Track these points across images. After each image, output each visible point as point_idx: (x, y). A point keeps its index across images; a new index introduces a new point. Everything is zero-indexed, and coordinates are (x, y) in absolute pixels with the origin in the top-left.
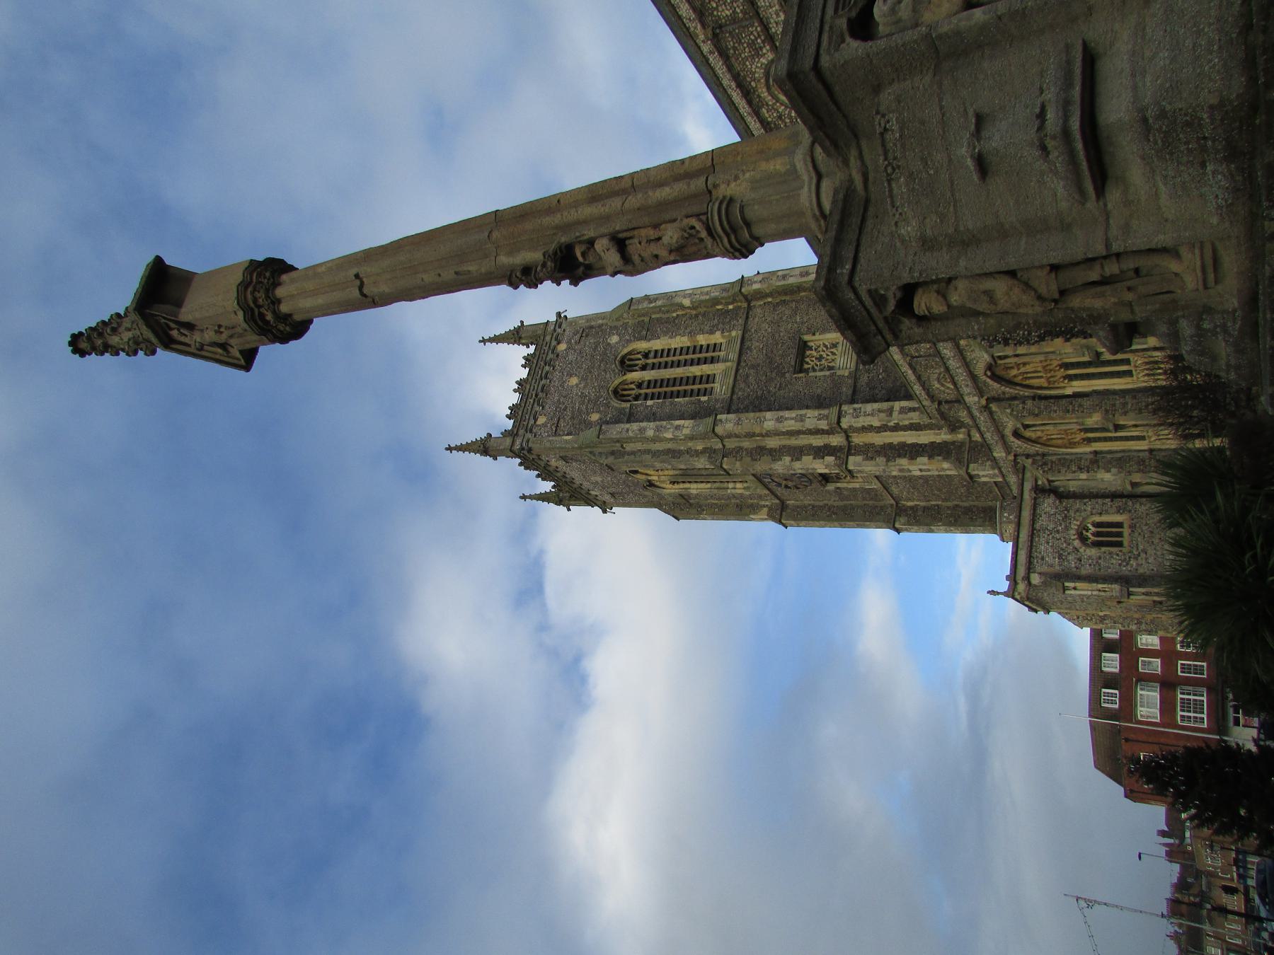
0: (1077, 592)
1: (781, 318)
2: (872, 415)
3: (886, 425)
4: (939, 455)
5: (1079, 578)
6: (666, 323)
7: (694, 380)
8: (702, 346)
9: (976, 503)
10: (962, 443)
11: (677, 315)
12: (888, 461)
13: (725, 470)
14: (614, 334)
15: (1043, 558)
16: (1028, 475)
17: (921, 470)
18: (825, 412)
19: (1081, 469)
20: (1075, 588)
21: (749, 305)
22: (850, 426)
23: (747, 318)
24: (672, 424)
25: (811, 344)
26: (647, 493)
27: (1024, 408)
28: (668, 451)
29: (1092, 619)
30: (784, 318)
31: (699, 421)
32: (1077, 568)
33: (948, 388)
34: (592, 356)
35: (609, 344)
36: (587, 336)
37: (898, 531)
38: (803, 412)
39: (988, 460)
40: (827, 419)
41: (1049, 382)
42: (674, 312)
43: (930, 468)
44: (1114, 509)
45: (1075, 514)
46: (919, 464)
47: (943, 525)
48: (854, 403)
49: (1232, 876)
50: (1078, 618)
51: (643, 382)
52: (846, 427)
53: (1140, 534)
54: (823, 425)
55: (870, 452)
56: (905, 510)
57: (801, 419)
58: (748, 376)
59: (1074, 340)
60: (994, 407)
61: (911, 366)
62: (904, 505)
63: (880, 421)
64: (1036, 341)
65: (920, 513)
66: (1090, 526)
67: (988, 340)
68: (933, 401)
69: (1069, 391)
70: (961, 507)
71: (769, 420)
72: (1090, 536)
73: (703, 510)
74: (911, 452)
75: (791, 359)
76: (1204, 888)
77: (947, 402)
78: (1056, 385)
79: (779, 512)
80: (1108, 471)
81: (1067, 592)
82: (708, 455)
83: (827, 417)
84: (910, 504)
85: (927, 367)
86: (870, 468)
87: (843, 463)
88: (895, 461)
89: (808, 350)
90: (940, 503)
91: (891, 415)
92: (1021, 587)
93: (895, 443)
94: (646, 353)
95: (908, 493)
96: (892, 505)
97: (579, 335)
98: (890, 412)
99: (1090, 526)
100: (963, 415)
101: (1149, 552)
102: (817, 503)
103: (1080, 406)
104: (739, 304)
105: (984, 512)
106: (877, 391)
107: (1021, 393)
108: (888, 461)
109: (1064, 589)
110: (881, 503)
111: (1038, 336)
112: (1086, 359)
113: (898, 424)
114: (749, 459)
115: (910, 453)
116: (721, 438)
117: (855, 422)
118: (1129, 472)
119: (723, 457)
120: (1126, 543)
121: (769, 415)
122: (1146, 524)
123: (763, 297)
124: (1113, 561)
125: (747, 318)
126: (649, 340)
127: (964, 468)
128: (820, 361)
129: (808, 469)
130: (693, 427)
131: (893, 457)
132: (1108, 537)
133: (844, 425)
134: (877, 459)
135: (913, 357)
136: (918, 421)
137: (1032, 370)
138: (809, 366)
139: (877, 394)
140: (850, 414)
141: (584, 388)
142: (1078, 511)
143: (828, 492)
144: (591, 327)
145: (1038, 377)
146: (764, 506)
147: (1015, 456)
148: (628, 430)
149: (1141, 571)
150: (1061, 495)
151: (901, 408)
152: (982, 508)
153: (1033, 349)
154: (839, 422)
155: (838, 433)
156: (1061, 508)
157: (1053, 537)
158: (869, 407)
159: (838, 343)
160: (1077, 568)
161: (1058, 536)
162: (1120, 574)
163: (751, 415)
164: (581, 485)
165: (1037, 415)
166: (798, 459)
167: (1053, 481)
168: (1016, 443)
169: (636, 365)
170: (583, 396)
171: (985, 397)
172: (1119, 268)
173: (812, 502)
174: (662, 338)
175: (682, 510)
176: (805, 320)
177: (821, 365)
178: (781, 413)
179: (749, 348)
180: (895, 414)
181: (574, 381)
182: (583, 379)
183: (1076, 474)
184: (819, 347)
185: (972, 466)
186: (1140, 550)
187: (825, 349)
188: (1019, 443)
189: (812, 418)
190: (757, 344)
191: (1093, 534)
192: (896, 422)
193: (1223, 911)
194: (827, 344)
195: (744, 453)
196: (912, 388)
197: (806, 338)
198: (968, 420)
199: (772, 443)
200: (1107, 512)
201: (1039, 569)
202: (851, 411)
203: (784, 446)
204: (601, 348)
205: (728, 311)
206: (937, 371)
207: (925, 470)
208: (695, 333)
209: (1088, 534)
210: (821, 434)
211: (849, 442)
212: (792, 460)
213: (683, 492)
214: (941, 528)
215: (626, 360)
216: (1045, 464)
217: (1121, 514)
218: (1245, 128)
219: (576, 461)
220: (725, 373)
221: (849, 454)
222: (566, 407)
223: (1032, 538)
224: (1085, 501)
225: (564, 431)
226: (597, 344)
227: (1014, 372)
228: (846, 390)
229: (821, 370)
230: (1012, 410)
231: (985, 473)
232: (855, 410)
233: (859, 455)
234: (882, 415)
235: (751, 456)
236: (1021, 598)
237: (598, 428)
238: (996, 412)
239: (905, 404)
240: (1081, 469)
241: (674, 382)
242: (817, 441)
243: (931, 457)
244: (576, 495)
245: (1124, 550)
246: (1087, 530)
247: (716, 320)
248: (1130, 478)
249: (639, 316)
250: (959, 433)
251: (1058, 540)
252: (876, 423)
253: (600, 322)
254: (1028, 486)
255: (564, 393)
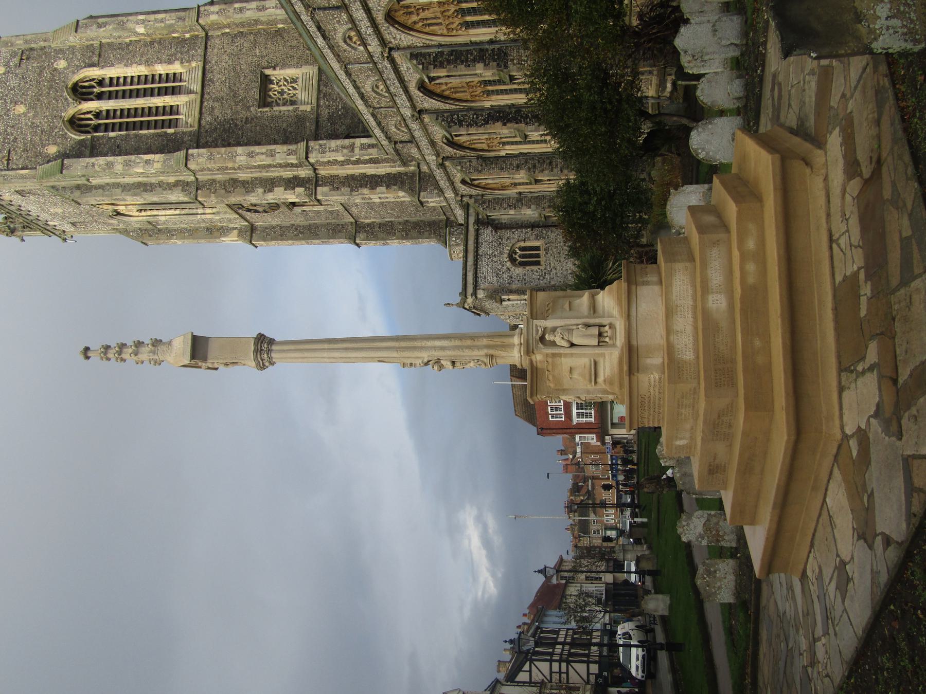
0: (511, 302)
1: (240, 50)
2: (337, 151)
3: (350, 160)
4: (395, 185)
5: (511, 292)
6: (119, 49)
7: (157, 110)
8: (160, 75)
9: (423, 218)
10: (413, 174)
11: (131, 41)
12: (352, 191)
13: (200, 202)
14: (60, 59)
15: (485, 278)
16: (471, 211)
17: (380, 198)
18: (293, 147)
19: (510, 206)
20: (509, 300)
21: (207, 34)
22: (317, 161)
23: (206, 48)
24: (141, 159)
25: (273, 78)
26: (112, 221)
27: (470, 165)
28: (139, 185)
29: (519, 318)
30: (244, 51)
31: (168, 156)
32: (510, 284)
33: (403, 131)
34: (38, 82)
35: (56, 69)
36: (28, 59)
37: (358, 245)
38: (273, 147)
39: (435, 188)
40: (296, 154)
41: (489, 146)
42: (127, 37)
43: (388, 196)
44: (534, 236)
45: (507, 240)
46: (379, 194)
47: (397, 239)
48: (319, 140)
49: (609, 477)
50: (510, 317)
51: (101, 111)
52: (313, 161)
53: (551, 255)
54: (293, 160)
55: (335, 183)
56: (364, 227)
57: (272, 154)
58: (213, 108)
59: (509, 125)
60: (447, 163)
61: (373, 115)
62: (362, 223)
63: (343, 156)
64: (482, 124)
65: (377, 229)
66: (518, 251)
67: (447, 121)
68: (390, 142)
69: (503, 153)
70: (410, 222)
71: (241, 154)
72: (518, 258)
73: (173, 235)
74: (371, 182)
75: (255, 93)
76: (590, 489)
77: (402, 142)
78: (494, 148)
79: (249, 233)
80: (530, 208)
81: (503, 303)
82: (181, 187)
83: (294, 152)
84: (367, 221)
85: (386, 116)
86: (336, 198)
87: (312, 194)
88: (358, 191)
89: (270, 84)
90: (393, 219)
91: (353, 151)
92: (470, 300)
93: (357, 174)
94: (100, 80)
95: (366, 212)
96: (352, 223)
97: (18, 58)
98: (352, 148)
99: (518, 251)
100: (414, 151)
101: (558, 268)
102: (284, 224)
103: (511, 164)
104: (196, 33)
105: (429, 225)
106: (338, 127)
107: (469, 154)
108: (352, 191)
109: (501, 301)
110: (343, 222)
111: (484, 120)
112: (518, 139)
113: (359, 159)
114: (223, 191)
115: (370, 183)
116: (194, 173)
117: (321, 158)
118: (543, 208)
119: (197, 189)
120: (542, 263)
121: (240, 150)
122: (556, 247)
123: (220, 28)
124: (532, 274)
125: (206, 48)
126: (103, 67)
127: (417, 196)
128: (282, 95)
129: (280, 199)
130: (164, 161)
131: (356, 187)
132: (529, 258)
133: (312, 160)
134: (342, 190)
135: (375, 108)
136: (377, 156)
137: (432, 15)
138: (272, 100)
139: (338, 130)
140: (316, 150)
141: (34, 116)
142: (508, 239)
143: (295, 214)
144: (32, 49)
145: (481, 143)
146: (234, 229)
147: (462, 196)
148: (93, 165)
149: (552, 283)
150: (497, 226)
151: (362, 144)
152: (428, 222)
153: (481, 130)
154: (307, 158)
155: (306, 166)
156: (496, 237)
157: (492, 261)
158: (334, 143)
159: (297, 78)
160: (510, 284)
161: (495, 259)
162: (539, 286)
163: (223, 150)
164: (38, 216)
165: (480, 171)
166: (270, 191)
167: (490, 216)
168: (463, 189)
169: (92, 93)
170: (33, 126)
171: (442, 157)
172: (599, 330)
173: (280, 223)
174: (116, 66)
175: (150, 236)
176: (265, 54)
177: (284, 99)
178: (252, 148)
179: (211, 80)
180: (357, 150)
181: (21, 109)
182: (30, 107)
183: (507, 210)
184: (280, 81)
185: (422, 194)
186: (552, 266)
187: (285, 83)
188: (465, 187)
189: (281, 154)
190: (219, 76)
191: (520, 256)
192: (358, 157)
193: (604, 505)
194: (288, 78)
195: (218, 185)
196: (373, 131)
197: (268, 72)
198: (417, 156)
199: (243, 176)
200: (529, 239)
201: (482, 286)
202: (317, 147)
203: (256, 178)
204: (47, 74)
205: (185, 40)
206: (395, 119)
207: (383, 198)
208: (152, 62)
209: (516, 256)
210: (291, 167)
211: (316, 174)
212: (265, 191)
213: (151, 219)
214: (395, 241)
215: (78, 88)
216: (484, 202)
217: (539, 240)
218: (632, 118)
219: (34, 194)
220: (190, 104)
221: (317, 185)
222: (16, 138)
223: (477, 262)
224: (513, 230)
225: (17, 165)
226: (42, 69)
227: (414, 18)
228: (310, 126)
229: (284, 105)
230: (462, 167)
231: (433, 201)
232: (321, 146)
233: (326, 186)
234: (345, 151)
235: (225, 188)
236: (469, 307)
237: (59, 161)
238: (449, 167)
239: (364, 141)
240: (510, 206)
241: (136, 112)
242: (288, 174)
243: (388, 187)
244: (31, 226)
245: (542, 268)
246: (516, 253)
247: (173, 50)
248: (544, 213)
249: (87, 40)
250: (411, 166)
251: (495, 262)
252: (341, 158)
253: (42, 44)
254: (472, 220)
255: (11, 123)
